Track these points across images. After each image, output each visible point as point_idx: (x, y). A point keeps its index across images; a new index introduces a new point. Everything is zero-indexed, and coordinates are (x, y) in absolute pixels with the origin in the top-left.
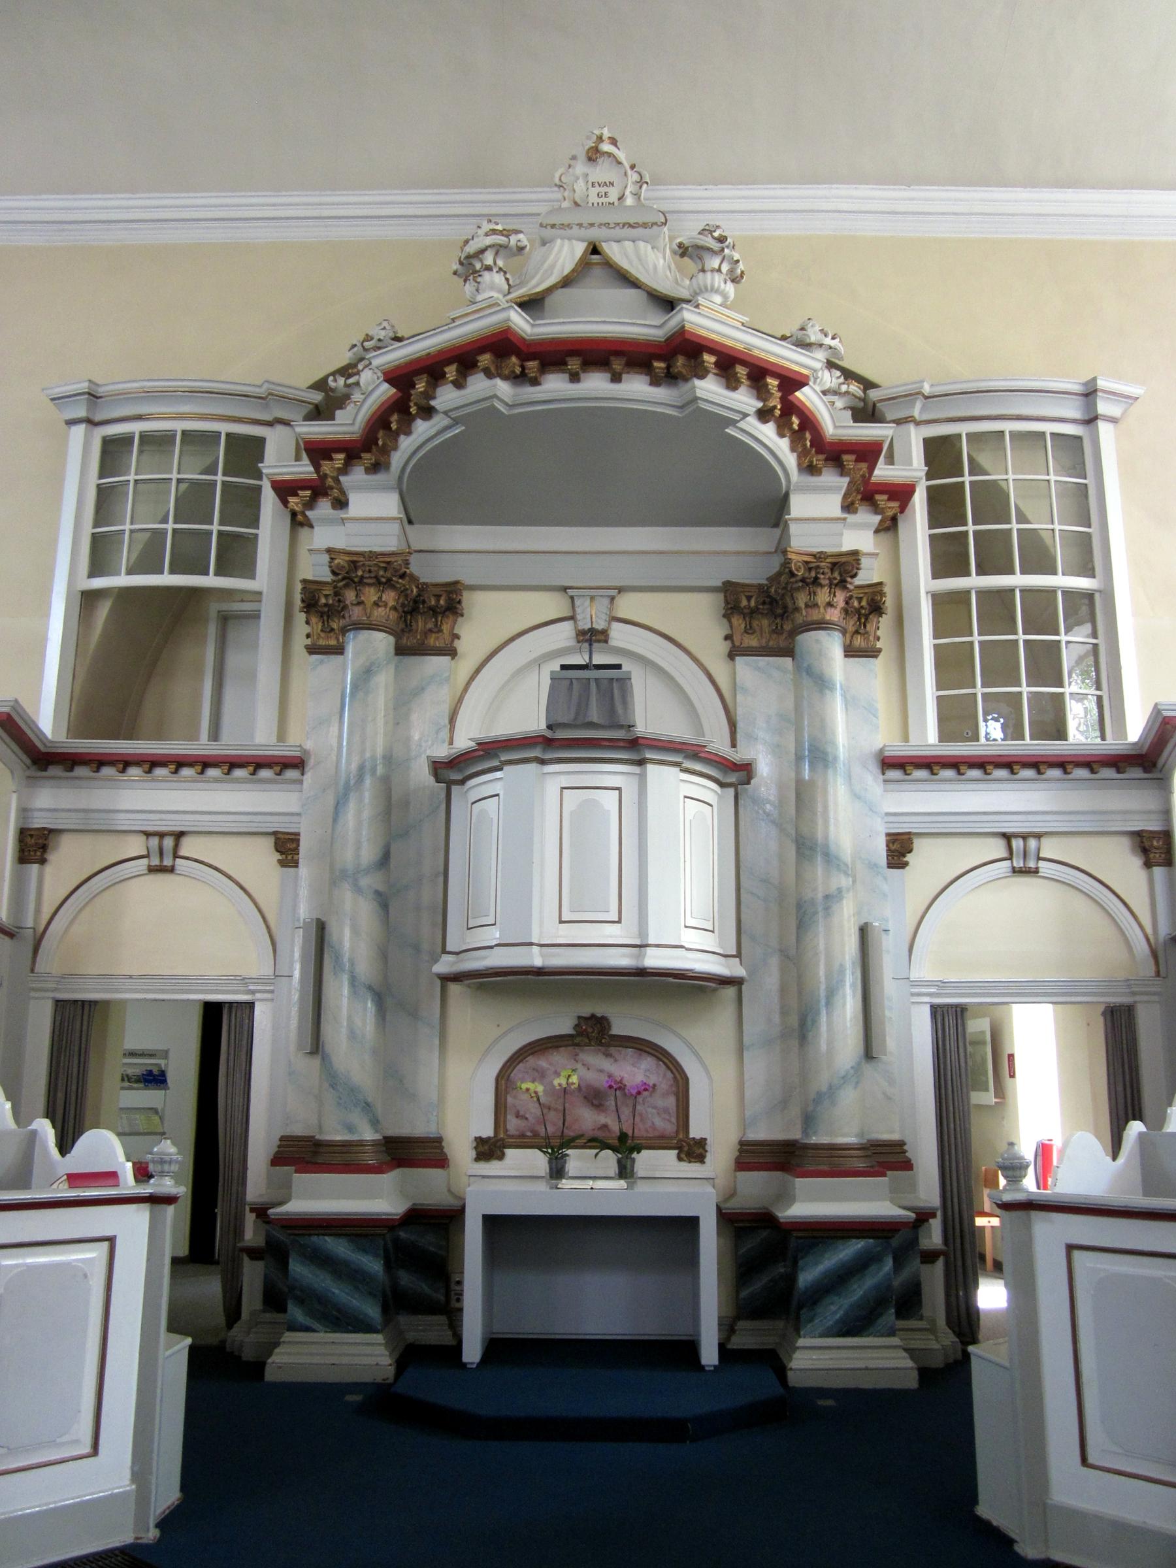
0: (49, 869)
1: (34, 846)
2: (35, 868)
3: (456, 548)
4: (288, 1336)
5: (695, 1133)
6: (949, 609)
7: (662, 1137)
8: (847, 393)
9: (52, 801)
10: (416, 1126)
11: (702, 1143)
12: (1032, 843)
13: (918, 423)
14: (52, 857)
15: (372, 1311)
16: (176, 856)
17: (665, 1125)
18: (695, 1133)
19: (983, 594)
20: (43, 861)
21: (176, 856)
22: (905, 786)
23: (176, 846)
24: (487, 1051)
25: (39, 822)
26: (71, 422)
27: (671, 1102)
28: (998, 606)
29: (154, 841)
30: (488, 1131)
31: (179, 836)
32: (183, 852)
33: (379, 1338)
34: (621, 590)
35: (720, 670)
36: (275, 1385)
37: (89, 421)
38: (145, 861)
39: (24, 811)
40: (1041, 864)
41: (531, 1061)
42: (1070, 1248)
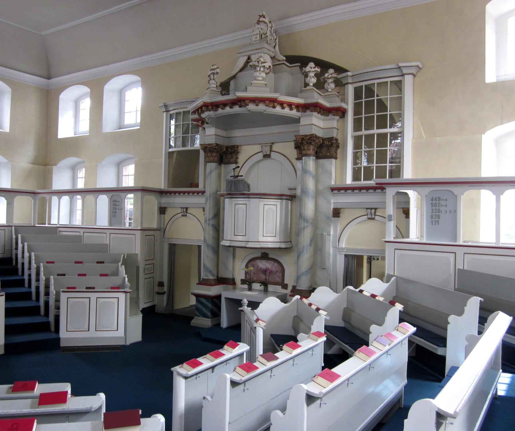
0: (166, 215)
1: (162, 210)
2: (163, 215)
3: (239, 135)
4: (196, 317)
5: (286, 282)
6: (357, 141)
7: (278, 283)
8: (331, 78)
9: (165, 200)
10: (229, 276)
11: (287, 285)
12: (373, 211)
13: (351, 83)
14: (166, 213)
15: (209, 314)
16: (186, 213)
17: (279, 280)
18: (286, 282)
19: (379, 135)
20: (164, 214)
21: (375, 215)
22: (338, 195)
23: (375, 213)
24: (244, 259)
25: (163, 206)
26: (164, 112)
27: (281, 274)
28: (369, 138)
29: (369, 211)
30: (244, 278)
31: (376, 209)
32: (188, 212)
33: (210, 320)
34: (273, 143)
35: (294, 161)
36: (192, 326)
37: (166, 111)
38: (366, 217)
39: (160, 203)
40: (376, 217)
41: (252, 262)
42: (68, 298)
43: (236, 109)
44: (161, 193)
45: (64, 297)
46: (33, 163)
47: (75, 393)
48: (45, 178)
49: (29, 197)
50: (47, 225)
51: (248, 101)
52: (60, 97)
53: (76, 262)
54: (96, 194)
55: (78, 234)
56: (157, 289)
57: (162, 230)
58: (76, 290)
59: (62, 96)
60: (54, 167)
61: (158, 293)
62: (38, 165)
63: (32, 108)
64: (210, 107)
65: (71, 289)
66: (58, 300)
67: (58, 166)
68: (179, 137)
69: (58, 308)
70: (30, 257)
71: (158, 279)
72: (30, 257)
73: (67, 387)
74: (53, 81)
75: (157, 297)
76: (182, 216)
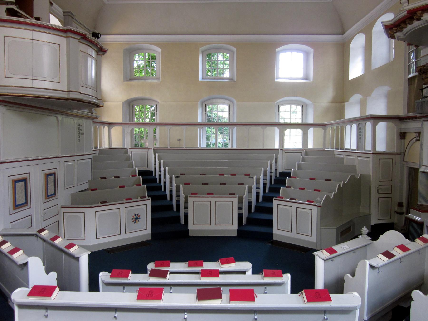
0: (406, 140)
1: (403, 135)
2: (403, 140)
25: (403, 131)
43: (416, 24)
44: (401, 119)
45: (190, 200)
46: (332, 102)
47: (254, 272)
48: (340, 112)
49: (320, 128)
50: (330, 149)
51: (420, 12)
52: (350, 46)
53: (310, 179)
54: (263, 127)
55: (342, 156)
56: (396, 209)
57: (402, 154)
58: (198, 196)
59: (352, 45)
60: (346, 103)
61: (397, 213)
62: (336, 103)
63: (330, 60)
64: (394, 29)
65: (194, 194)
66: (186, 202)
67: (349, 102)
68: (413, 62)
69: (186, 208)
70: (165, 170)
71: (398, 201)
72: (165, 170)
73: (247, 266)
74: (346, 34)
75: (396, 216)
76: (417, 140)
